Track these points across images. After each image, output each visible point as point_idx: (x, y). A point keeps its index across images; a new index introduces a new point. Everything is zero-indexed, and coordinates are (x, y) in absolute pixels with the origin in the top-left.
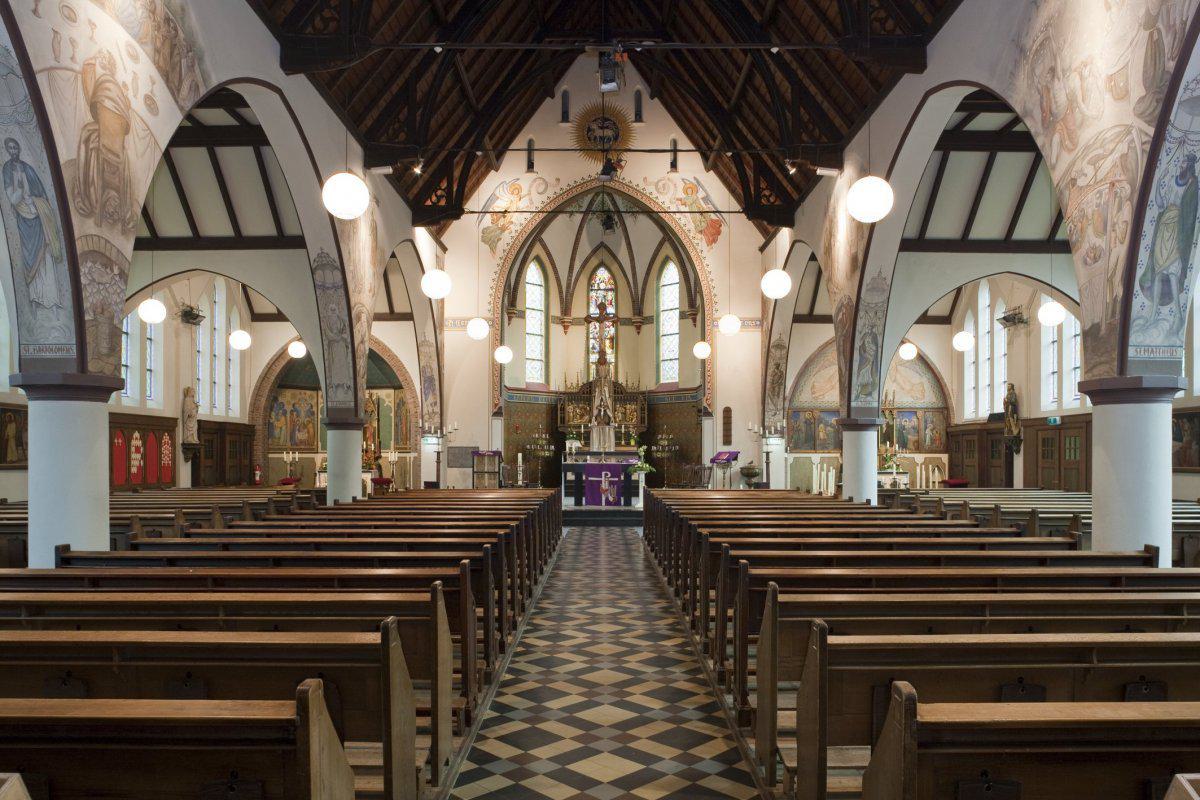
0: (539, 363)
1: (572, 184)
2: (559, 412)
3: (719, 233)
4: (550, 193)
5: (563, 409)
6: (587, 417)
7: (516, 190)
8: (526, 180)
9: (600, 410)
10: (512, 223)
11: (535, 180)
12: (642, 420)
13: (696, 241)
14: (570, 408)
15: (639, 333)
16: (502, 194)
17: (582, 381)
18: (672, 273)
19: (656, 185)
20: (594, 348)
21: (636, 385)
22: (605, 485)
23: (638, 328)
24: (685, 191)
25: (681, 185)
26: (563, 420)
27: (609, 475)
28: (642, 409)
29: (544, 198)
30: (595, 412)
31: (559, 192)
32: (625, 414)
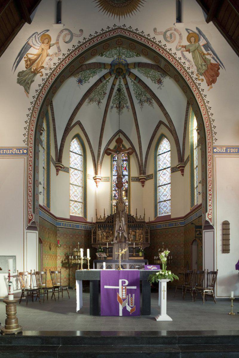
0: (80, 204)
1: (94, 34)
2: (92, 235)
3: (218, 75)
4: (75, 42)
5: (95, 233)
6: (111, 238)
7: (45, 38)
8: (54, 31)
9: (119, 233)
10: (43, 67)
11: (62, 31)
12: (147, 239)
13: (198, 82)
14: (99, 232)
15: (143, 186)
16: (35, 43)
17: (108, 214)
18: (165, 146)
19: (165, 34)
20: (115, 196)
21: (142, 217)
22: (122, 294)
23: (143, 183)
24: (189, 39)
25: (185, 35)
26: (95, 239)
27: (127, 283)
28: (147, 233)
29: (70, 46)
30: (116, 234)
31: (82, 41)
32: (135, 235)
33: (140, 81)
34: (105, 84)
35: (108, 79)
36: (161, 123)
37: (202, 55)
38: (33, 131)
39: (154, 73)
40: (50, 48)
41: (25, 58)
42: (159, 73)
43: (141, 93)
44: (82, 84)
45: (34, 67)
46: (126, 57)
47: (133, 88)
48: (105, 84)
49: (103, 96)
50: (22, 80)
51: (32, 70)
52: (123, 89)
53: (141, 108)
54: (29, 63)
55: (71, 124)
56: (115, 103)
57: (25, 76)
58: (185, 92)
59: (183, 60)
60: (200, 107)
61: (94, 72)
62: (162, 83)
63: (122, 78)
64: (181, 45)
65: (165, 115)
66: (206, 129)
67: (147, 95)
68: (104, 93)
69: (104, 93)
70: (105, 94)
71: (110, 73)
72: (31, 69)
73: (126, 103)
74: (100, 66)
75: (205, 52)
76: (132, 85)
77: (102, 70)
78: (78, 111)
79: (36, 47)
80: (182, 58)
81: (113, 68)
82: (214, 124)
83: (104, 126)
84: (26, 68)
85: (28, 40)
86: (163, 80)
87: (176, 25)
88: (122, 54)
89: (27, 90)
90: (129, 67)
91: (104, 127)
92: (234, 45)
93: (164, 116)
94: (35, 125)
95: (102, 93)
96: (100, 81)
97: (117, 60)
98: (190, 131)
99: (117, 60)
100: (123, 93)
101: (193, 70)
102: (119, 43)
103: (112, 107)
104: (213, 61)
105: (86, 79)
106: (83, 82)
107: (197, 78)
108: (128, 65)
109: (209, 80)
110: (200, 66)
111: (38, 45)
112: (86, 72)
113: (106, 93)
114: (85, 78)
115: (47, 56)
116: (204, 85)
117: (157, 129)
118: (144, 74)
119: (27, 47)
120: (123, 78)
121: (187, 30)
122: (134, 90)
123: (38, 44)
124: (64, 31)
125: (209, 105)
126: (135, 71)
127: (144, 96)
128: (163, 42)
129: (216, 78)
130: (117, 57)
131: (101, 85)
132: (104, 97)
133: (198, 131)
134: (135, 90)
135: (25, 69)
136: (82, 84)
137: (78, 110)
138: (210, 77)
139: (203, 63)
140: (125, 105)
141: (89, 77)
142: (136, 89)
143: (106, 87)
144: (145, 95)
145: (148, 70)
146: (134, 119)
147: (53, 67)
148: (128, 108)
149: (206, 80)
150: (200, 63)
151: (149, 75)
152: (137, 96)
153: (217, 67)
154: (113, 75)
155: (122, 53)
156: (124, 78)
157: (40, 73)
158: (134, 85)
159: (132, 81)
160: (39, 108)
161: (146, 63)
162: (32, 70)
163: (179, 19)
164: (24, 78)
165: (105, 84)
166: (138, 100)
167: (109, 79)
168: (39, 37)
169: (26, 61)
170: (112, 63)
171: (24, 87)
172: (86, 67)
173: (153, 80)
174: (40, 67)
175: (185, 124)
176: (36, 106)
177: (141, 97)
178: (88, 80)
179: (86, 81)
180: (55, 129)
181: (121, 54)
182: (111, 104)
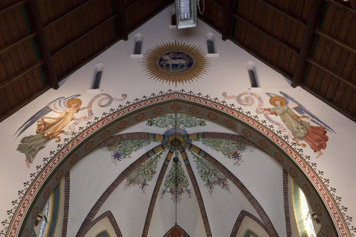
3: (326, 139)
10: (63, 132)
13: (297, 147)
33: (206, 155)
34: (154, 161)
35: (158, 154)
36: (244, 214)
37: (296, 118)
38: (21, 216)
39: (226, 145)
40: (77, 112)
41: (38, 122)
42: (233, 145)
43: (209, 172)
44: (120, 159)
45: (48, 131)
46: (185, 126)
47: (197, 165)
48: (155, 159)
49: (151, 176)
50: (26, 147)
51: (46, 135)
52: (182, 167)
53: (211, 192)
54: (43, 127)
55: (94, 216)
56: (168, 186)
57: (32, 141)
58: (279, 161)
59: (268, 124)
60: (310, 179)
61: (139, 145)
62: (239, 158)
63: (179, 153)
64: (263, 107)
65: (249, 200)
66: (331, 212)
67: (218, 174)
68: (152, 171)
69: (152, 171)
70: (153, 173)
71: (162, 146)
72: (44, 133)
73: (186, 185)
74: (147, 137)
75: (298, 114)
76: (195, 161)
77: (150, 143)
78: (109, 195)
79: (58, 111)
80: (267, 121)
81: (166, 139)
82: (342, 204)
83: (151, 218)
84: (37, 132)
85: (49, 104)
86: (240, 154)
87: (252, 90)
88: (179, 124)
89: (29, 160)
90: (190, 138)
91: (150, 220)
92: (338, 107)
93: (249, 202)
94: (28, 207)
95: (150, 172)
96: (147, 155)
97: (173, 130)
98: (297, 223)
99: (173, 130)
100: (181, 171)
101: (287, 134)
102: (175, 107)
103: (164, 192)
104: (313, 124)
105: (126, 153)
106: (121, 157)
107: (295, 143)
108: (188, 135)
109: (315, 145)
110: (295, 130)
111: (61, 109)
112: (127, 145)
113: (155, 172)
114: (124, 152)
115: (72, 119)
116: (308, 151)
117: (238, 223)
118: (212, 147)
119: (46, 110)
120: (181, 152)
121: (268, 94)
122: (198, 168)
123: (63, 108)
124: (102, 95)
125: (325, 176)
126: (199, 144)
127: (213, 176)
128: (237, 106)
129: (325, 143)
130: (172, 126)
131: (148, 160)
132: (152, 177)
133: (315, 217)
134: (200, 168)
135: (35, 134)
136: (120, 159)
137: (110, 194)
138: (315, 142)
139: (300, 127)
140: (184, 189)
141: (132, 151)
142: (201, 166)
143: (156, 164)
144: (215, 175)
145: (218, 140)
146: (200, 207)
147: (77, 131)
148: (189, 192)
149: (309, 144)
150: (294, 125)
151: (219, 148)
152: (203, 176)
153: (322, 131)
154: (166, 149)
155: (180, 122)
156: (183, 152)
157: (57, 138)
158: (197, 161)
159: (195, 156)
160: (43, 182)
161: (214, 133)
162: (46, 135)
163: (255, 84)
164: (29, 144)
165: (154, 161)
166: (205, 181)
167: (161, 154)
168: (65, 102)
169: (39, 126)
170: (164, 133)
171: (26, 154)
172: (128, 137)
173: (226, 153)
174: (59, 131)
175: (286, 212)
176: (38, 180)
177: (209, 177)
178: (130, 154)
179: (125, 155)
180: (67, 222)
181: (178, 123)
182: (162, 187)
